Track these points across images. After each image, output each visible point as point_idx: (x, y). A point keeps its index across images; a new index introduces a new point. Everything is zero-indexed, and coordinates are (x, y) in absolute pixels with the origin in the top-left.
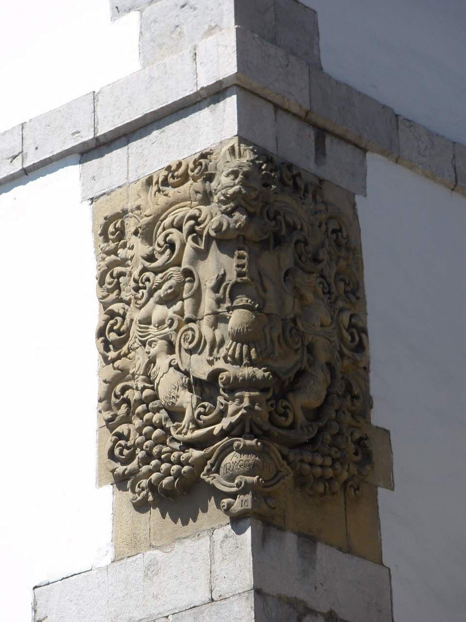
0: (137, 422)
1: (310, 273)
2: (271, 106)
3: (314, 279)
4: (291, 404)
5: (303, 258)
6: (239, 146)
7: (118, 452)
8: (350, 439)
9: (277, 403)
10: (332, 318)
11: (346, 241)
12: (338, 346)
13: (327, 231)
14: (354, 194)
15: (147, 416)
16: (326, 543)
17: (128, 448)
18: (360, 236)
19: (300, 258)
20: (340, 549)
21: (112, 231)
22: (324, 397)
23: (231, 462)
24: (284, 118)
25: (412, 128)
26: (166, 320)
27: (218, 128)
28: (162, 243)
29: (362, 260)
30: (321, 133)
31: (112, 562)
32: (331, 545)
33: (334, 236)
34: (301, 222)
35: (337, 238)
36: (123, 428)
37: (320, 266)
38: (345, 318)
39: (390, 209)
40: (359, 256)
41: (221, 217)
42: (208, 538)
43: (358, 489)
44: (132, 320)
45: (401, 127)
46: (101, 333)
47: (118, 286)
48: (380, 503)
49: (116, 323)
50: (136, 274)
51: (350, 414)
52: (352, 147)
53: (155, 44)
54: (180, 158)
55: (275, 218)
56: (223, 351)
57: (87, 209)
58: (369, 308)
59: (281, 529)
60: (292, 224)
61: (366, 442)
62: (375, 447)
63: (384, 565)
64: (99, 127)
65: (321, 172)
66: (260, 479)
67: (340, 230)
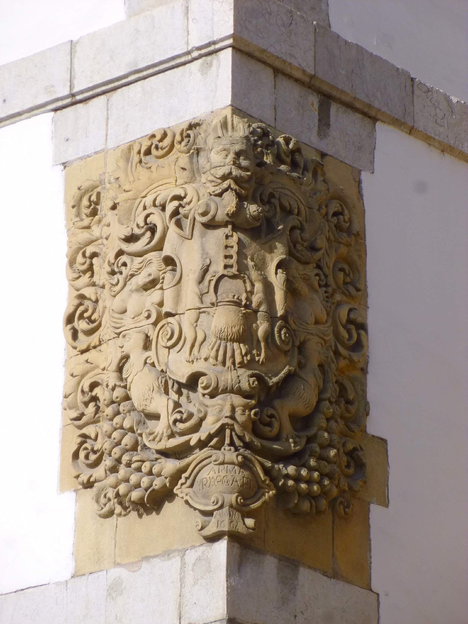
0: (105, 426)
1: (307, 263)
2: (270, 72)
3: (311, 271)
4: (277, 413)
5: (299, 247)
6: (232, 117)
7: (84, 454)
8: (342, 450)
9: (262, 411)
10: (328, 314)
11: (348, 225)
12: (333, 344)
13: (327, 214)
14: (360, 172)
15: (117, 419)
16: (310, 567)
17: (95, 452)
18: (364, 219)
19: (295, 246)
20: (325, 574)
21: (88, 205)
22: (315, 404)
23: (208, 477)
24: (285, 85)
25: (430, 93)
26: (143, 312)
28: (142, 224)
29: (365, 246)
30: (327, 98)
31: (72, 577)
32: (315, 569)
33: (335, 220)
34: (298, 206)
35: (338, 222)
36: (90, 430)
37: (318, 255)
38: (343, 313)
39: (401, 194)
40: (363, 241)
41: (208, 200)
42: (178, 558)
43: (348, 507)
44: (105, 307)
45: (417, 92)
46: (70, 320)
47: (91, 268)
48: (372, 522)
49: (86, 311)
50: (111, 256)
51: (343, 422)
52: (360, 116)
54: (165, 126)
55: (269, 202)
56: (206, 351)
57: (58, 174)
58: (371, 301)
59: (260, 552)
60: (288, 208)
61: (360, 453)
62: (370, 459)
63: (372, 591)
64: (75, 82)
65: (323, 146)
66: (239, 498)
67: (342, 213)
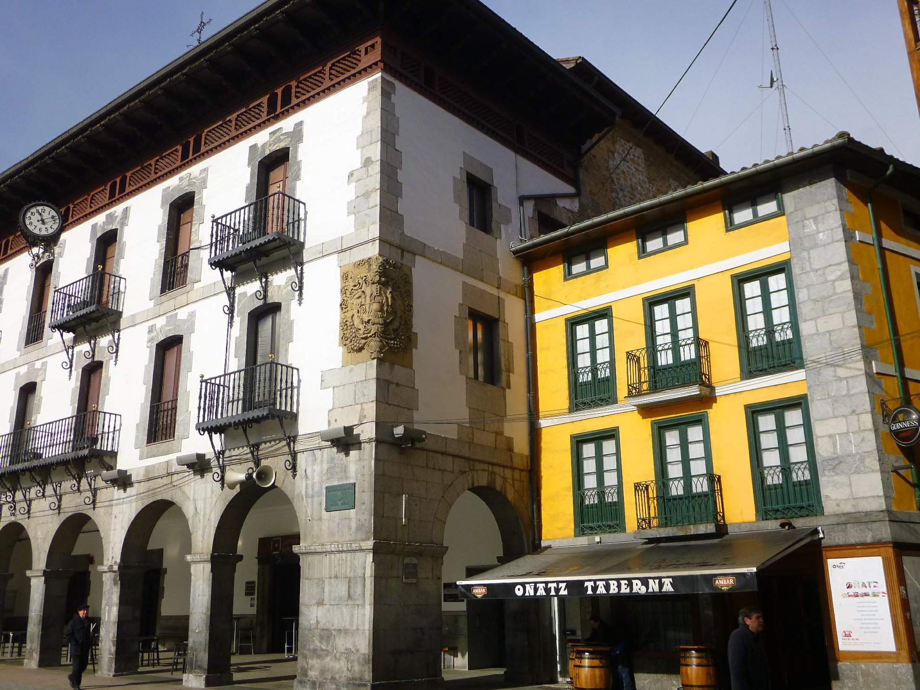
7: (344, 338)
21: (345, 277)
24: (392, 248)
27: (373, 250)
30: (403, 251)
53: (359, 225)
57: (339, 269)
